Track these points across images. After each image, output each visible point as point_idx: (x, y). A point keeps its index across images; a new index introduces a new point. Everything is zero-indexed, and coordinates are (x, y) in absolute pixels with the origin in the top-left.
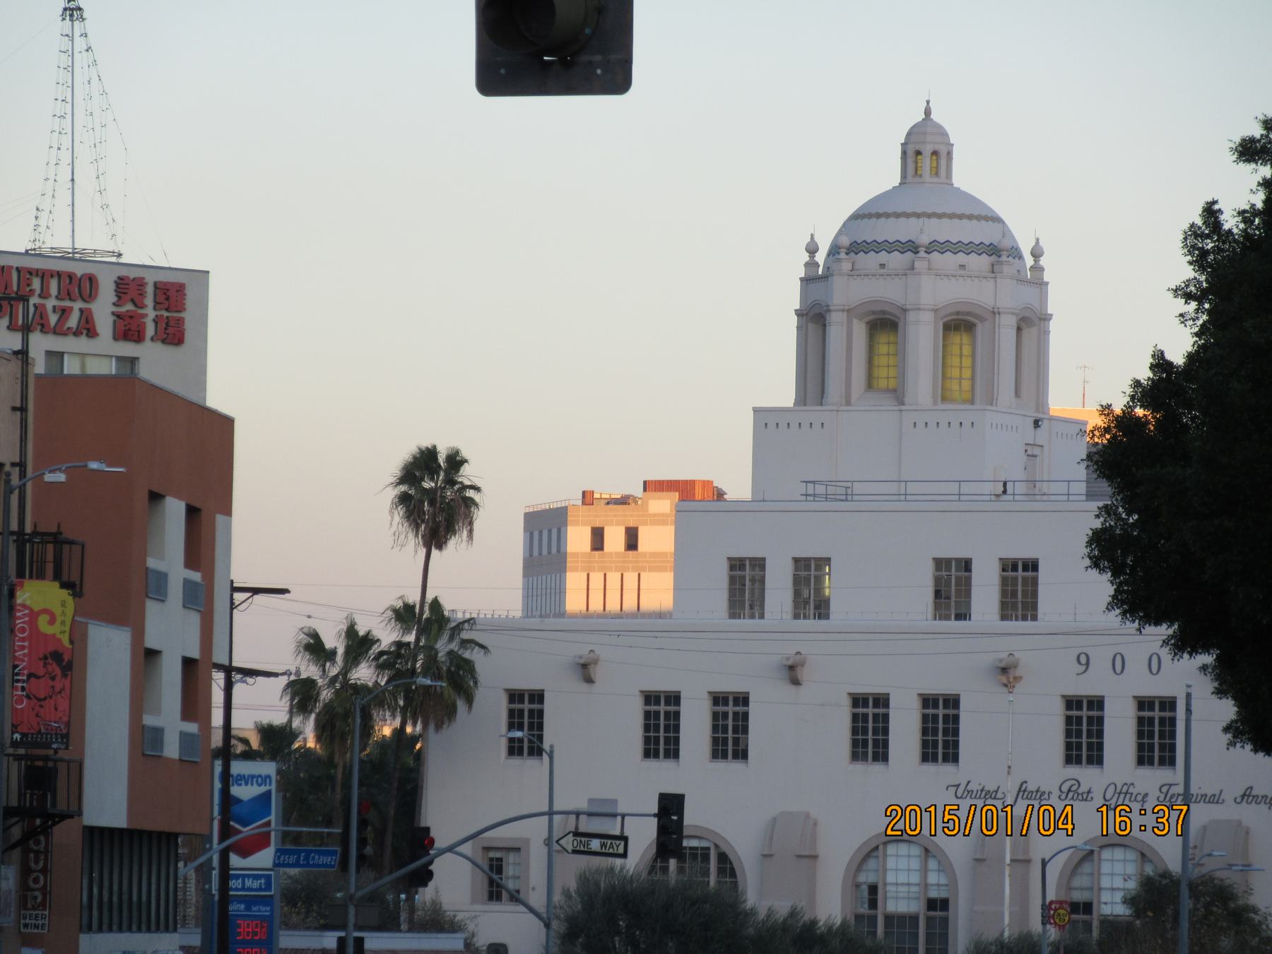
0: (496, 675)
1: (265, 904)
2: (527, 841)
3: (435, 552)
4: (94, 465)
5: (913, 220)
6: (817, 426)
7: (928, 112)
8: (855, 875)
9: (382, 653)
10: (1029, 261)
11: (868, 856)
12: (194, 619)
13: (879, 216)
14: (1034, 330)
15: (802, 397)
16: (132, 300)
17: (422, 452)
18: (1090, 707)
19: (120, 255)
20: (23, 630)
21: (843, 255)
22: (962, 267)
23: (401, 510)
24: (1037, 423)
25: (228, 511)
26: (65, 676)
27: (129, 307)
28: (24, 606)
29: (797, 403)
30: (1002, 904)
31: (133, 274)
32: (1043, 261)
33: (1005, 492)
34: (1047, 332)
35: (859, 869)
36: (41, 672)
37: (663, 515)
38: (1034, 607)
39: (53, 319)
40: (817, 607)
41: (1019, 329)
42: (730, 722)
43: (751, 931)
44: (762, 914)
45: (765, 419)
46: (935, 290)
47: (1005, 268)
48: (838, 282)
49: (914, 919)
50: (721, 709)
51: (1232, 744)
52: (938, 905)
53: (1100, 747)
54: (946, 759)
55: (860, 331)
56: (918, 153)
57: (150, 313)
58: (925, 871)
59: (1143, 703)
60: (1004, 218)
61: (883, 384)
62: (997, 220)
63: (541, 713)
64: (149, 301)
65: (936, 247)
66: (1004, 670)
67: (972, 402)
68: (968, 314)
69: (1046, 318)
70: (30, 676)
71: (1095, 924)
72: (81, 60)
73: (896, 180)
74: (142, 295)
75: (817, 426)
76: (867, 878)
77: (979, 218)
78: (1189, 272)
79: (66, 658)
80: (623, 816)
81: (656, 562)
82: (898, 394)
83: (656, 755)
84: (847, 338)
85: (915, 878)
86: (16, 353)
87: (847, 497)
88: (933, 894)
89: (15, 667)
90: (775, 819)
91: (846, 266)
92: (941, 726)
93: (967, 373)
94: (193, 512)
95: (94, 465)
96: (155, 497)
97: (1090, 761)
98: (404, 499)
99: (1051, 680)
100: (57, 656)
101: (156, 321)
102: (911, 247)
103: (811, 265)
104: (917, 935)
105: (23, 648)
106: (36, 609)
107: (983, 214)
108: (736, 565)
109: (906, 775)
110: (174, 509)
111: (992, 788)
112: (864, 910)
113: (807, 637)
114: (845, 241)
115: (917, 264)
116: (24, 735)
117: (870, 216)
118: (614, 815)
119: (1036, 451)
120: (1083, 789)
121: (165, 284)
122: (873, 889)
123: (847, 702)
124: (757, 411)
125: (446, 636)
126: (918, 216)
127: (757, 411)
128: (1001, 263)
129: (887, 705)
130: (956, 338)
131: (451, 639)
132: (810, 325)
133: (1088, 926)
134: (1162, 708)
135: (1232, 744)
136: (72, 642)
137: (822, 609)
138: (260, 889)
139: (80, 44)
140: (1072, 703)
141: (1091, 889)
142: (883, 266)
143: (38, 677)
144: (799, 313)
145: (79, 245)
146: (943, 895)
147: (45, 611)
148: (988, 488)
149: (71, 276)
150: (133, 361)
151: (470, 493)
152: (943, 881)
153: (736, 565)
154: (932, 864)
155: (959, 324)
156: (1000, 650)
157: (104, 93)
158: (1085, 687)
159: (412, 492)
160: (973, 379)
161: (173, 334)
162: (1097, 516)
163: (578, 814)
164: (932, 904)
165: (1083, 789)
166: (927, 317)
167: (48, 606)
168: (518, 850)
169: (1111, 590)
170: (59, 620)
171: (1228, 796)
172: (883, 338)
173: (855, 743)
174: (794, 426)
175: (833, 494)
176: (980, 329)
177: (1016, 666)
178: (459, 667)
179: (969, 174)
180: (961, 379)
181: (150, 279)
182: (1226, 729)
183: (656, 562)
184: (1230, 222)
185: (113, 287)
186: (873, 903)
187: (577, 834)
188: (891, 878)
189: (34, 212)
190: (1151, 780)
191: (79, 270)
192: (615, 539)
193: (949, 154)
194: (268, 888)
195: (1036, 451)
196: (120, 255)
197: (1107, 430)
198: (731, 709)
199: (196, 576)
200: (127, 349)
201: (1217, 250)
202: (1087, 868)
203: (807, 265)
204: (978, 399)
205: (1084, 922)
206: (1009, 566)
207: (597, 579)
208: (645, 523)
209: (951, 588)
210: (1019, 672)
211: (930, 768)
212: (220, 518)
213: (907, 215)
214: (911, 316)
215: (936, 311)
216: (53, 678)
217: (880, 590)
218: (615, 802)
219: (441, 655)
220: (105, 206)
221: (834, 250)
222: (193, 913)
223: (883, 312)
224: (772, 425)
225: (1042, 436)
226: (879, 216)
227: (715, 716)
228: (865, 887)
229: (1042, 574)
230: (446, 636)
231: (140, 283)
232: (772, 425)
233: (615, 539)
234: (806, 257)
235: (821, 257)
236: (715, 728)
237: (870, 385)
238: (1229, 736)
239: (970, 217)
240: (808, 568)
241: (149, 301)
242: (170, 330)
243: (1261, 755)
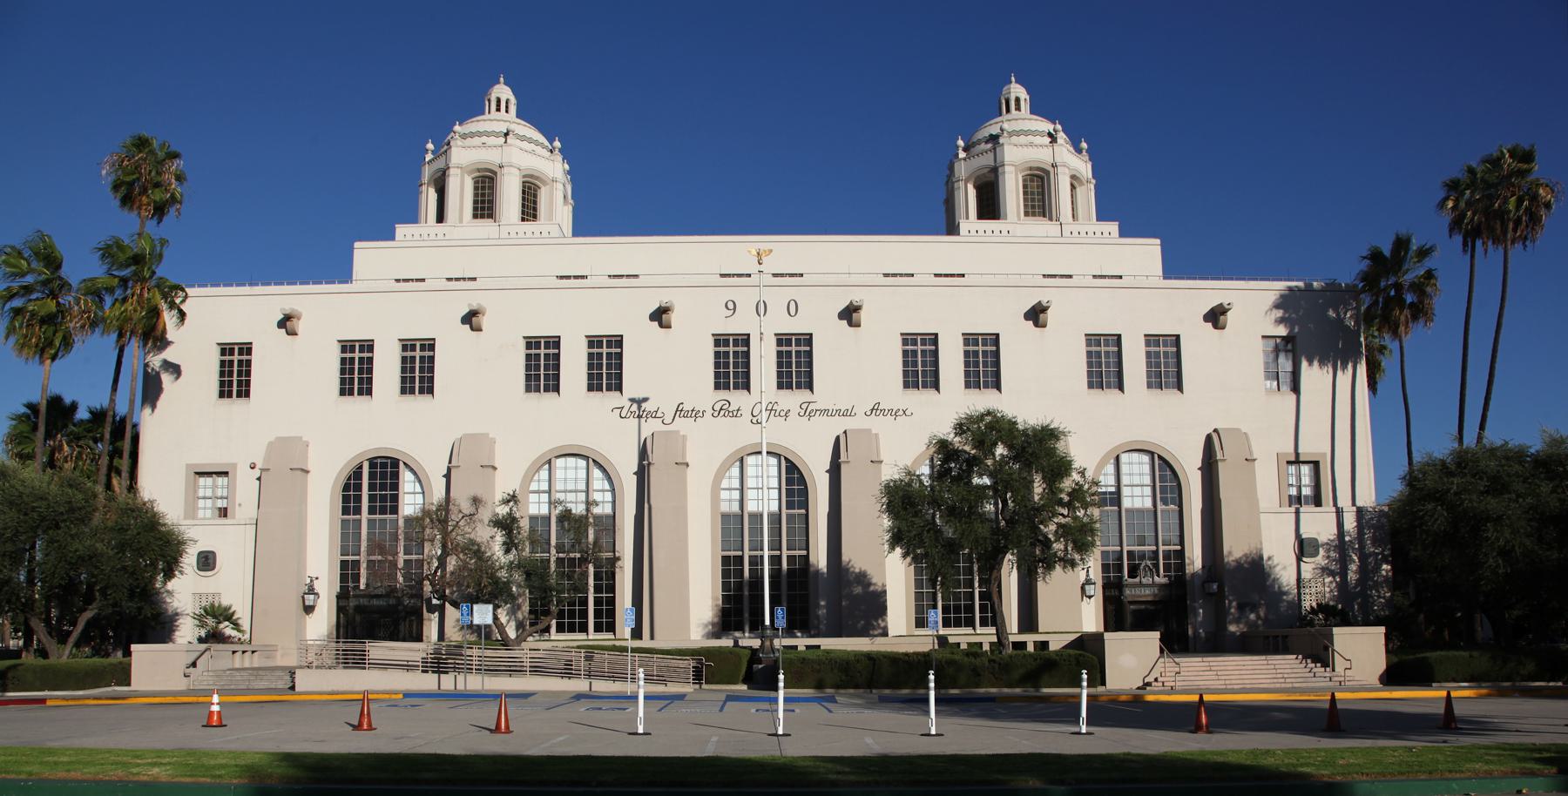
2: (234, 466)
23: (1364, 265)
59: (782, 340)
71: (401, 523)
83: (412, 392)
109: (577, 411)
123: (522, 344)
140: (720, 340)
168: (226, 474)
171: (860, 411)
222: (744, 643)
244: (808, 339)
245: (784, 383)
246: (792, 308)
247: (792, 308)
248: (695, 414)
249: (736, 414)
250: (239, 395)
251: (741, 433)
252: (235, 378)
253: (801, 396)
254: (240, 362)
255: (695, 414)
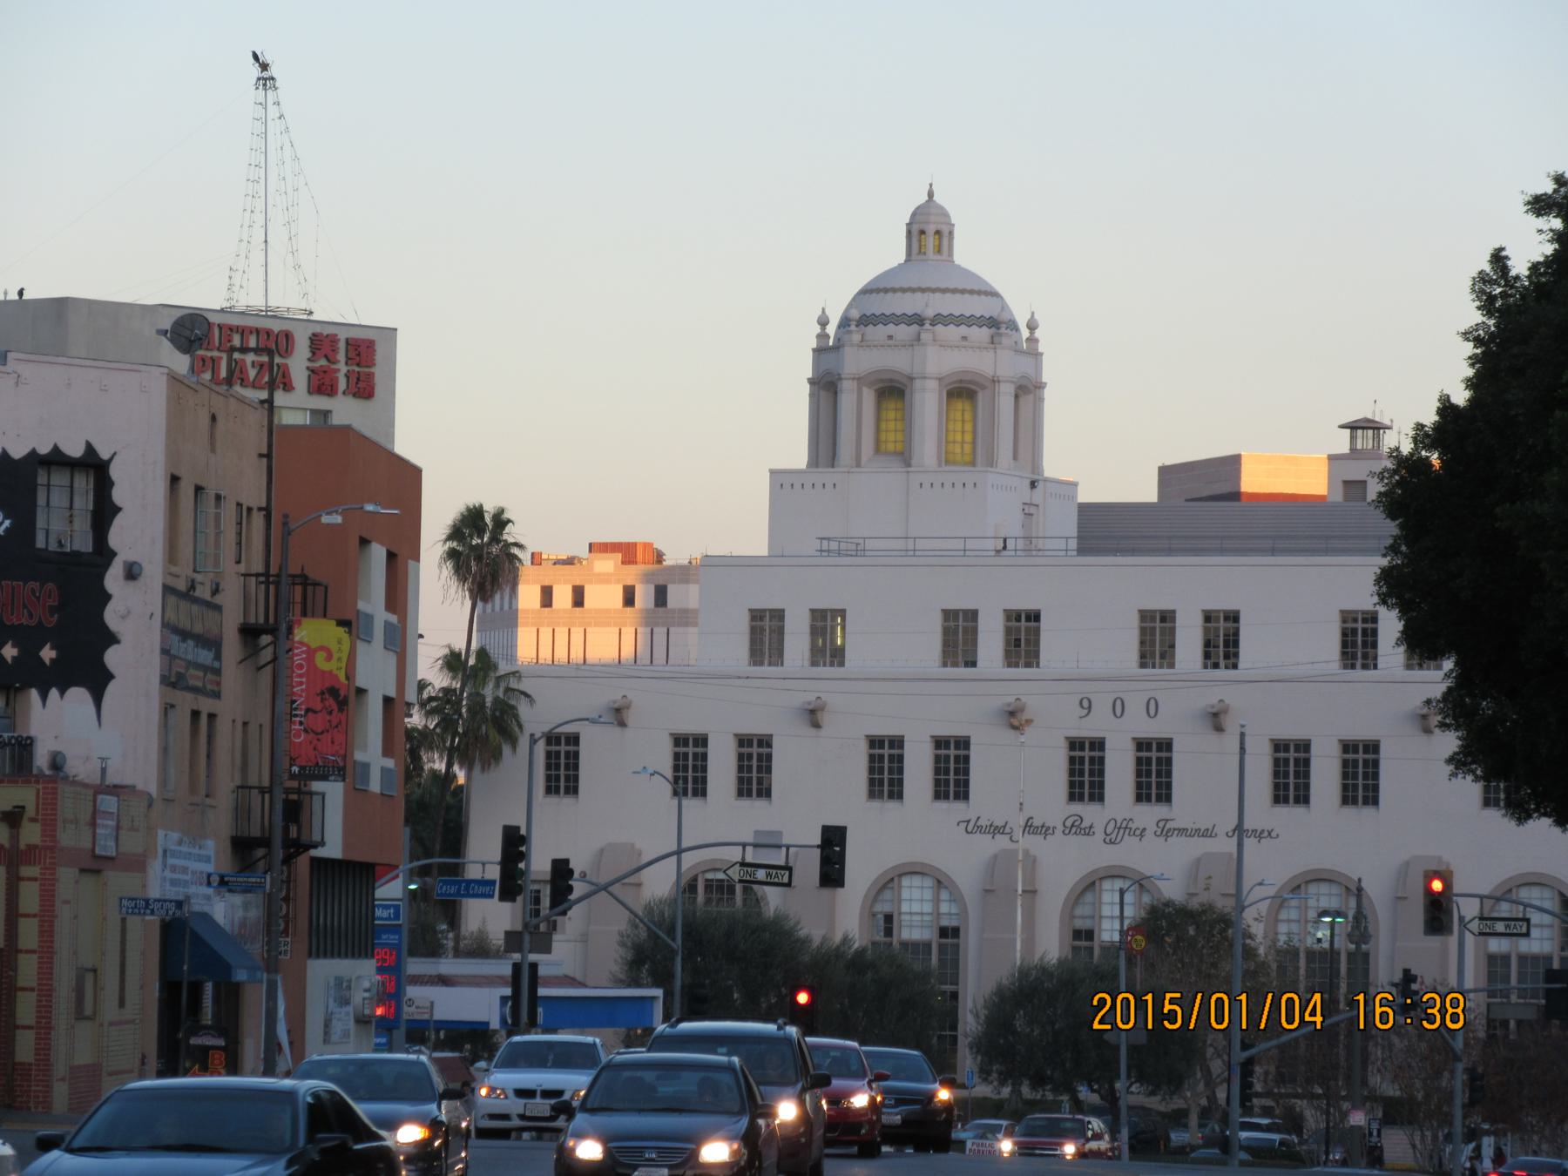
0: (535, 719)
1: (395, 933)
3: (480, 604)
4: (370, 507)
5: (919, 295)
6: (829, 486)
7: (931, 194)
8: (872, 906)
9: (431, 699)
10: (1025, 333)
11: (1085, 890)
12: (392, 659)
13: (886, 291)
14: (1031, 397)
15: (814, 461)
16: (326, 356)
17: (469, 510)
18: (1159, 749)
19: (311, 313)
20: (301, 667)
21: (853, 327)
22: (964, 338)
23: (450, 565)
24: (1033, 484)
25: (417, 559)
26: (341, 710)
27: (323, 362)
28: (302, 644)
29: (810, 465)
30: (1014, 932)
31: (327, 331)
32: (1037, 334)
33: (1005, 548)
34: (1042, 400)
35: (875, 900)
36: (318, 706)
37: (608, 574)
38: (1037, 655)
39: (252, 373)
40: (833, 656)
41: (1016, 397)
42: (755, 763)
43: (806, 958)
44: (816, 942)
45: (781, 480)
46: (942, 359)
47: (1005, 340)
48: (848, 353)
49: (927, 946)
50: (745, 750)
51: (1453, 775)
52: (949, 933)
53: (1101, 785)
54: (957, 797)
55: (869, 397)
56: (922, 232)
57: (342, 368)
58: (936, 901)
59: (1142, 745)
60: (1001, 291)
61: (891, 447)
62: (994, 294)
63: (576, 755)
64: (341, 356)
65: (939, 319)
66: (1012, 714)
67: (973, 463)
68: (970, 382)
69: (1040, 386)
70: (308, 710)
72: (274, 127)
73: (901, 257)
74: (335, 351)
75: (829, 486)
76: (883, 907)
77: (979, 293)
78: (1477, 317)
79: (342, 693)
80: (788, 847)
81: (603, 618)
82: (905, 457)
83: (557, 792)
84: (856, 404)
85: (928, 908)
86: (262, 402)
87: (859, 551)
88: (945, 923)
89: (293, 702)
90: (602, 851)
91: (856, 338)
92: (952, 766)
93: (968, 438)
94: (391, 556)
95: (370, 507)
96: (364, 542)
97: (1092, 798)
98: (452, 555)
99: (1057, 720)
100: (333, 692)
101: (347, 376)
102: (918, 320)
103: (823, 336)
104: (1297, 968)
105: (301, 683)
106: (314, 645)
107: (976, 288)
108: (756, 615)
110: (378, 553)
111: (999, 823)
112: (880, 937)
113: (825, 685)
114: (855, 314)
115: (923, 336)
116: (302, 768)
117: (878, 291)
118: (779, 847)
119: (1032, 510)
120: (1086, 824)
121: (356, 340)
122: (889, 918)
124: (773, 472)
125: (491, 685)
126: (923, 290)
127: (773, 472)
128: (1000, 335)
129: (769, 745)
130: (959, 405)
131: (497, 686)
132: (822, 393)
133: (1091, 949)
134: (1159, 749)
135: (1453, 775)
136: (347, 678)
137: (838, 656)
138: (389, 918)
139: (273, 111)
140: (1075, 744)
141: (1093, 917)
142: (890, 337)
143: (315, 712)
144: (811, 382)
145: (273, 303)
146: (954, 923)
147: (322, 648)
148: (990, 544)
149: (268, 333)
150: (326, 414)
151: (515, 551)
152: (954, 911)
153: (756, 615)
154: (944, 895)
155: (962, 391)
156: (1006, 695)
157: (296, 158)
158: (1087, 729)
159: (460, 549)
160: (974, 443)
161: (363, 388)
162: (1384, 556)
163: (744, 845)
164: (944, 932)
165: (1086, 824)
166: (932, 385)
167: (325, 644)
169: (1400, 626)
170: (336, 656)
172: (891, 404)
173: (872, 782)
174: (808, 486)
175: (843, 550)
176: (981, 397)
177: (1022, 710)
178: (502, 713)
179: (968, 253)
180: (963, 442)
181: (343, 335)
182: (1450, 761)
183: (603, 618)
184: (1519, 267)
185: (308, 343)
186: (889, 932)
187: (743, 864)
188: (905, 908)
189: (228, 273)
190: (1148, 814)
191: (276, 327)
192: (562, 597)
193: (951, 233)
194: (397, 917)
195: (1032, 510)
196: (311, 313)
197: (1395, 472)
198: (755, 750)
199: (393, 619)
200: (321, 402)
201: (1504, 295)
202: (1089, 897)
203: (818, 336)
204: (979, 459)
205: (1086, 948)
206: (1013, 616)
207: (546, 634)
208: (591, 582)
209: (959, 637)
210: (1025, 716)
211: (943, 805)
212: (411, 563)
213: (913, 290)
214: (918, 384)
215: (940, 379)
216: (330, 713)
217: (892, 640)
218: (780, 833)
219: (489, 701)
220: (297, 267)
221: (845, 322)
223: (891, 380)
224: (787, 486)
225: (1037, 497)
226: (886, 291)
227: (741, 757)
228: (881, 917)
229: (1044, 623)
230: (491, 685)
231: (333, 339)
232: (787, 486)
233: (562, 597)
234: (818, 329)
235: (831, 329)
236: (740, 769)
237: (878, 449)
238: (1452, 767)
239: (971, 292)
240: (824, 618)
241: (341, 356)
242: (361, 385)
243: (1470, 789)
244: (1166, 745)
245: (1142, 796)
246: (1152, 708)
247: (1152, 708)
248: (1046, 831)
249: (1088, 831)
250: (567, 792)
251: (1094, 854)
252: (886, 775)
253: (1159, 811)
254: (1366, 762)
255: (1046, 831)
